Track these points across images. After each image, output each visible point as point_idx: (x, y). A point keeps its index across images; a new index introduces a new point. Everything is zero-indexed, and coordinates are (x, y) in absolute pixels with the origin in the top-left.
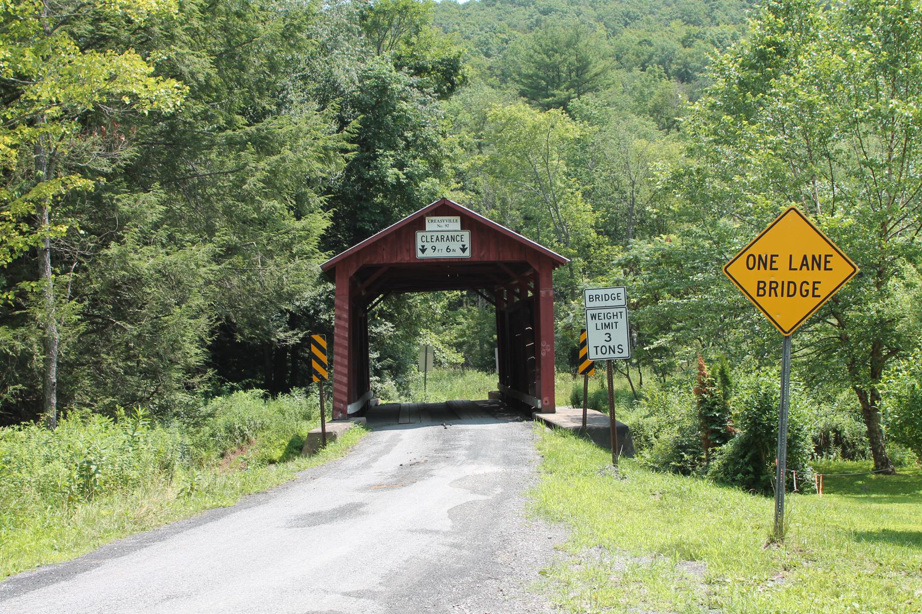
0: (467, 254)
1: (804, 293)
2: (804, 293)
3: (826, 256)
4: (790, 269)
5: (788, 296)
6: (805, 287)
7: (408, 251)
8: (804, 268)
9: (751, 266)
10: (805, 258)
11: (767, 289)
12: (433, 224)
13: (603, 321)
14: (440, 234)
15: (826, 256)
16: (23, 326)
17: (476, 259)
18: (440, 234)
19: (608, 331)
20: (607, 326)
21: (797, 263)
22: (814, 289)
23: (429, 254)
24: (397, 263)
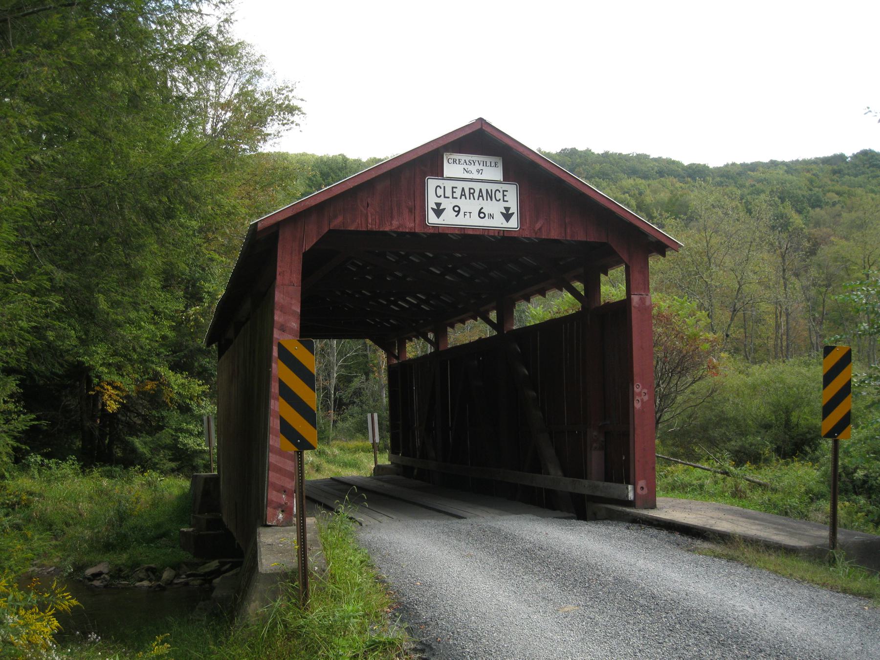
0: (514, 223)
7: (411, 211)
14: (467, 185)
17: (527, 234)
23: (448, 219)
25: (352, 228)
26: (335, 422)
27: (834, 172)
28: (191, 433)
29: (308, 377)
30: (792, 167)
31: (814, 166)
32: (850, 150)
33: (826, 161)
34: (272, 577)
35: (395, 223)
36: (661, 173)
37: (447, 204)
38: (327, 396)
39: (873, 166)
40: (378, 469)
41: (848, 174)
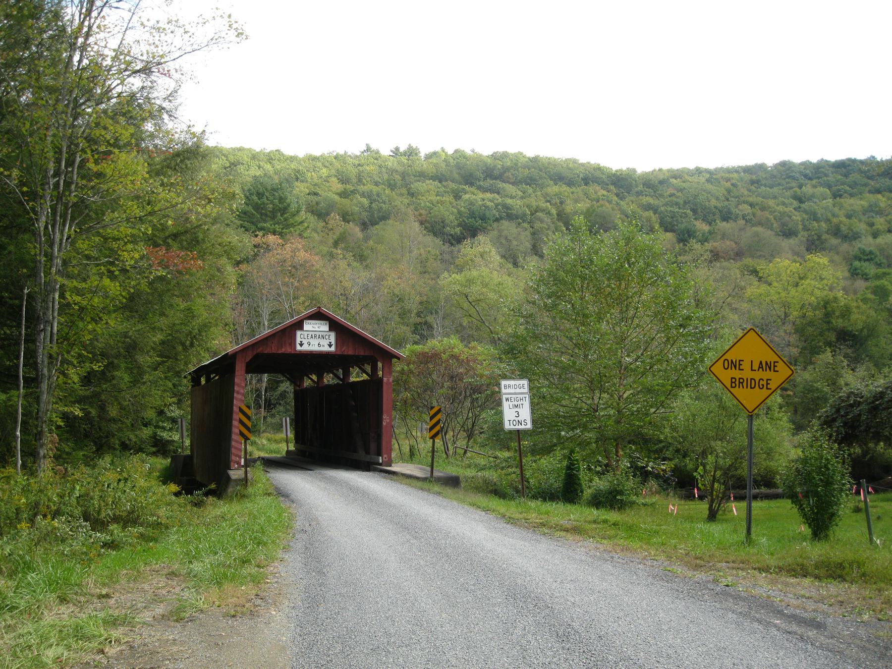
0: (333, 349)
1: (761, 387)
2: (761, 387)
3: (774, 362)
4: (752, 370)
5: (751, 388)
6: (761, 382)
7: (290, 345)
8: (761, 369)
9: (726, 367)
10: (761, 363)
11: (737, 383)
12: (309, 326)
13: (514, 403)
14: (313, 333)
15: (774, 362)
16: (80, 396)
17: (338, 353)
18: (313, 333)
19: (517, 409)
20: (516, 406)
21: (756, 367)
22: (767, 384)
23: (306, 348)
24: (283, 354)
25: (266, 352)
26: (265, 418)
27: (753, 182)
28: (164, 428)
29: (249, 418)
30: (713, 176)
31: (735, 175)
32: (771, 161)
33: (747, 170)
34: (236, 480)
35: (283, 350)
36: (586, 181)
37: (305, 342)
38: (259, 396)
39: (789, 177)
40: (288, 452)
41: (765, 186)
